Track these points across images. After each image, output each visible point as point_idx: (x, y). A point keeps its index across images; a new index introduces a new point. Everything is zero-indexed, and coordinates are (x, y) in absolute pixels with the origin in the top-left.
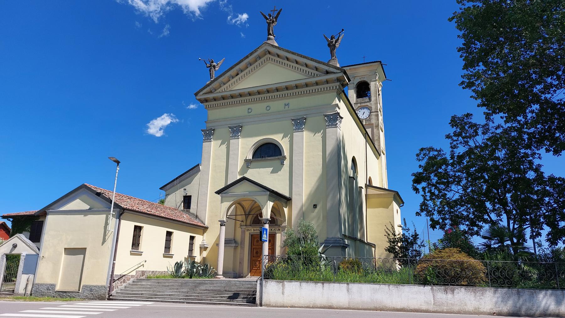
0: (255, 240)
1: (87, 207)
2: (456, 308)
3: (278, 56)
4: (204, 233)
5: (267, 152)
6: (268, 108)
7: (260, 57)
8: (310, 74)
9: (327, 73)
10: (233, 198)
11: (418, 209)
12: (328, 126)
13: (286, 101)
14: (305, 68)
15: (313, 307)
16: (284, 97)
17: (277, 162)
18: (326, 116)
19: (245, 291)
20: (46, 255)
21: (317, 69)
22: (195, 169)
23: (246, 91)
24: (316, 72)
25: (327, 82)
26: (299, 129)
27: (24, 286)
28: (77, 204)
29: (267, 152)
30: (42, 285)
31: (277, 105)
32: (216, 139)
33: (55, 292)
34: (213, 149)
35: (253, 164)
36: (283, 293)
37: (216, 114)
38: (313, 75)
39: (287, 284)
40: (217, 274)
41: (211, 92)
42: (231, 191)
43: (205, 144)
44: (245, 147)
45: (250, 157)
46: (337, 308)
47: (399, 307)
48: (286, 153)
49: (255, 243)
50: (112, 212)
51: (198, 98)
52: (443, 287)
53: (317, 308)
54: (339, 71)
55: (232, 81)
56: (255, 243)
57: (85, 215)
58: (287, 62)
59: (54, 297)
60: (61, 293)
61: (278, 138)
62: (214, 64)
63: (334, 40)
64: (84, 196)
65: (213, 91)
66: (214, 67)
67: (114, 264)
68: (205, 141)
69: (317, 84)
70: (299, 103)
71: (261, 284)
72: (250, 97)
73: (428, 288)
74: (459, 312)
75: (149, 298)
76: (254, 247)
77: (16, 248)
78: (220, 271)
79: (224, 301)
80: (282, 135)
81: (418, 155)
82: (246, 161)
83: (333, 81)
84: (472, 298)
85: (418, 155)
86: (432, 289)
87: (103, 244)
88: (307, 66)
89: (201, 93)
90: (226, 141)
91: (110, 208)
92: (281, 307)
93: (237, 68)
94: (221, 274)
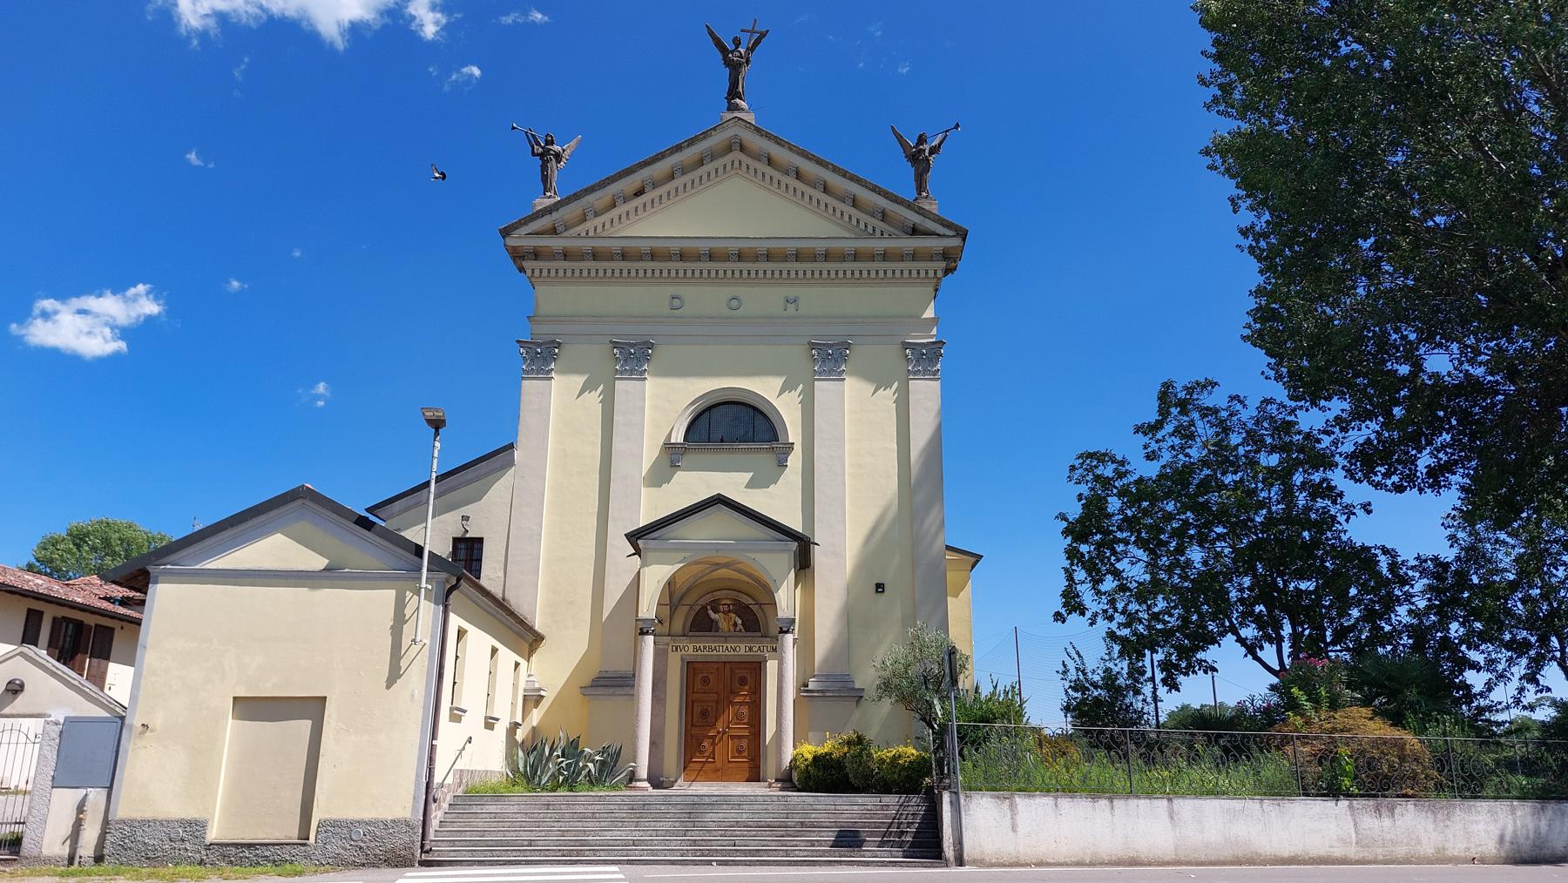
1: (320, 563)
2: (1401, 851)
3: (770, 162)
4: (530, 655)
5: (731, 426)
6: (734, 303)
7: (713, 155)
8: (862, 226)
9: (915, 231)
11: (1058, 605)
12: (915, 373)
13: (792, 292)
15: (1092, 864)
17: (766, 460)
18: (906, 346)
19: (877, 825)
20: (157, 721)
21: (884, 216)
22: (500, 456)
23: (675, 246)
24: (881, 225)
25: (914, 256)
26: (830, 372)
27: (66, 829)
28: (273, 549)
29: (731, 426)
30: (145, 823)
31: (763, 299)
32: (565, 371)
33: (209, 847)
34: (558, 408)
36: (1014, 828)
37: (560, 298)
38: (870, 229)
39: (1021, 802)
40: (632, 777)
41: (553, 231)
43: (530, 387)
44: (663, 403)
45: (678, 437)
46: (1150, 864)
47: (1286, 854)
48: (794, 434)
49: (698, 685)
50: (424, 585)
51: (511, 242)
52: (1371, 802)
53: (1102, 864)
55: (622, 209)
56: (698, 685)
57: (313, 587)
59: (201, 862)
60: (233, 850)
61: (765, 388)
62: (556, 148)
63: (926, 147)
64: (304, 526)
65: (559, 229)
66: (558, 157)
67: (433, 748)
68: (528, 374)
69: (885, 256)
70: (829, 301)
71: (956, 806)
72: (594, 264)
73: (1344, 803)
74: (1407, 861)
75: (570, 853)
76: (695, 696)
77: (21, 697)
78: (643, 772)
79: (824, 853)
80: (778, 382)
81: (1073, 468)
82: (668, 447)
83: (931, 257)
84: (1431, 826)
85: (1073, 468)
86: (1350, 807)
87: (391, 682)
88: (855, 203)
90: (602, 383)
91: (420, 569)
92: (1011, 865)
93: (638, 178)
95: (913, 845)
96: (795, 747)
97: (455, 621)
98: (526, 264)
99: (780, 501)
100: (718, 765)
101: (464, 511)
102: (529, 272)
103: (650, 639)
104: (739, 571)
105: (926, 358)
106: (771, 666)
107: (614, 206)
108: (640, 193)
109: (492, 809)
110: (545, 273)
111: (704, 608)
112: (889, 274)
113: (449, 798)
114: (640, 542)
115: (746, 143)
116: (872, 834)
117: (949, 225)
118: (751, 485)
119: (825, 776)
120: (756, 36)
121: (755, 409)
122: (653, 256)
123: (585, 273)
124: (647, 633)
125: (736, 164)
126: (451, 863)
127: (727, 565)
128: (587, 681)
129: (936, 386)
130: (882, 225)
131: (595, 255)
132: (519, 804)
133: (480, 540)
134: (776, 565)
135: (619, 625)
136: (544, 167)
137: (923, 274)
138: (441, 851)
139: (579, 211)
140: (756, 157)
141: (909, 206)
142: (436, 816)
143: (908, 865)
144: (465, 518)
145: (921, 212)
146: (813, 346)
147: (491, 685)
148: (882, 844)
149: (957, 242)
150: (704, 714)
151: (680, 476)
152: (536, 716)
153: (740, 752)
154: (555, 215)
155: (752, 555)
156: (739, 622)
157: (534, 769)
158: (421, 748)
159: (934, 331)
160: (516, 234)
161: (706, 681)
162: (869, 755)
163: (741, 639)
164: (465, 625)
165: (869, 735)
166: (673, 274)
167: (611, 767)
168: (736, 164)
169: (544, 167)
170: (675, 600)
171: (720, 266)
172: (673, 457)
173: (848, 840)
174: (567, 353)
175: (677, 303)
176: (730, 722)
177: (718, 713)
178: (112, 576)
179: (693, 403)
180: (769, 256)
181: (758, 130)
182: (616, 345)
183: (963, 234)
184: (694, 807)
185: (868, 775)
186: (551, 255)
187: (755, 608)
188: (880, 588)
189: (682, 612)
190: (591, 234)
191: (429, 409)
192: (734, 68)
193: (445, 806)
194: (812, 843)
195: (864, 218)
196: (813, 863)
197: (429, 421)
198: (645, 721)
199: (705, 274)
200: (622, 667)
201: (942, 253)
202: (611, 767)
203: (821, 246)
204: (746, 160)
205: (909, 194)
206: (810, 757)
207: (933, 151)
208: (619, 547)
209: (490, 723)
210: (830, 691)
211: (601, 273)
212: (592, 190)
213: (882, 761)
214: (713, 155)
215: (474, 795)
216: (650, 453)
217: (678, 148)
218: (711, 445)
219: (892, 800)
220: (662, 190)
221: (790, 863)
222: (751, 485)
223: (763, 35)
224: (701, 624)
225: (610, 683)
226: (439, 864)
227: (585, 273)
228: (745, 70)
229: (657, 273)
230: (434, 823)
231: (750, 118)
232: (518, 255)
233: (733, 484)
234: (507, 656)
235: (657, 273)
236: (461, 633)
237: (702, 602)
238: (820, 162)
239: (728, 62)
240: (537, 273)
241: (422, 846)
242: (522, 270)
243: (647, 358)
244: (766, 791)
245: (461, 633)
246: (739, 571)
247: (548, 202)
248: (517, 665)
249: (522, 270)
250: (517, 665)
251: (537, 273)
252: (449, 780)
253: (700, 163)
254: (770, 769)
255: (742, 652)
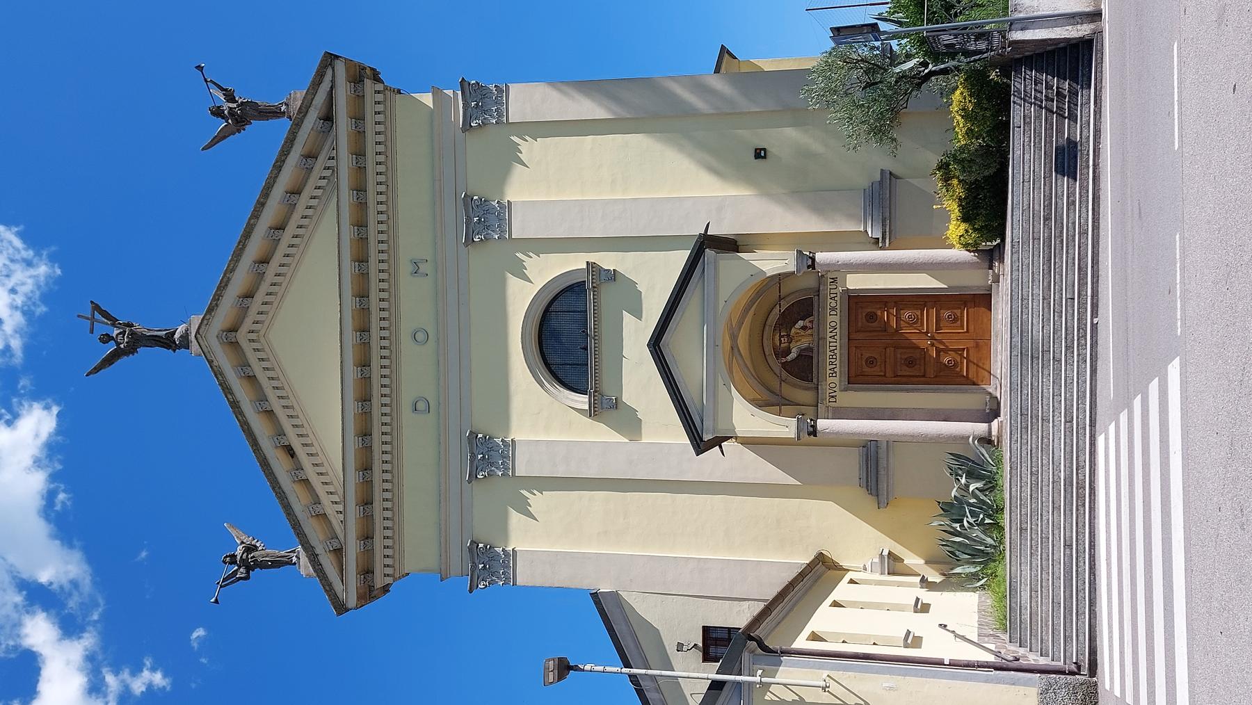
0: (866, 369)
3: (249, 295)
5: (567, 340)
6: (420, 336)
8: (323, 183)
9: (328, 117)
10: (721, 382)
12: (500, 115)
13: (405, 269)
14: (304, 200)
16: (389, 276)
17: (608, 295)
18: (467, 127)
21: (311, 156)
22: (606, 608)
24: (322, 160)
25: (358, 118)
26: (500, 218)
31: (414, 303)
34: (549, 542)
35: (608, 390)
37: (418, 544)
38: (328, 173)
40: (986, 440)
41: (338, 552)
42: (697, 401)
43: (524, 576)
44: (541, 420)
45: (582, 401)
48: (576, 262)
50: (757, 679)
51: (352, 601)
54: (329, 72)
55: (310, 472)
56: (876, 370)
58: (273, 267)
61: (520, 300)
62: (239, 551)
65: (336, 545)
66: (250, 549)
67: (953, 664)
68: (510, 579)
69: (359, 153)
78: (981, 428)
79: (1084, 188)
80: (513, 283)
82: (594, 412)
88: (296, 192)
89: (338, 587)
90: (518, 492)
91: (739, 684)
93: (271, 449)
94: (985, 425)
95: (1075, 79)
96: (951, 246)
97: (801, 643)
98: (379, 582)
99: (656, 276)
100: (971, 344)
101: (671, 649)
102: (389, 580)
103: (822, 424)
104: (741, 323)
105: (482, 102)
106: (855, 282)
107: (306, 482)
108: (290, 451)
109: (1026, 595)
110: (388, 561)
111: (784, 365)
112: (381, 148)
113: (1012, 647)
114: (706, 437)
115: (227, 325)
116: (1060, 131)
117: (320, 75)
118: (638, 315)
119: (986, 207)
120: (97, 316)
121: (547, 311)
122: (365, 433)
123: (388, 514)
124: (814, 427)
125: (253, 336)
126: (1093, 639)
127: (734, 338)
128: (870, 501)
129: (515, 90)
130: (321, 158)
131: (366, 502)
132: (1018, 566)
133: (706, 630)
134: (731, 278)
135: (802, 461)
136: (263, 565)
137: (380, 108)
138: (1077, 651)
139: (313, 522)
140: (243, 312)
141: (298, 124)
142: (1034, 659)
143: (1099, 81)
144: (680, 647)
145: (304, 110)
146: (469, 241)
147: (878, 606)
148: (1072, 117)
149: (340, 67)
150: (910, 363)
151: (629, 397)
152: (913, 560)
153: (955, 320)
154: (319, 550)
155: (721, 304)
156: (801, 323)
157: (975, 554)
158: (954, 677)
159: (449, 92)
160: (342, 596)
161: (871, 362)
162: (962, 149)
163: (821, 323)
164: (806, 632)
165: (934, 159)
166: (387, 410)
167: (974, 465)
168: (253, 336)
169: (263, 565)
170: (773, 399)
171: (375, 354)
172: (605, 406)
173: (1067, 160)
174: (483, 534)
175: (421, 406)
176: (921, 331)
177: (910, 347)
178: (562, 323)
179: (542, 385)
180: (362, 294)
181: (211, 310)
182: (473, 477)
183: (330, 59)
184: (1027, 355)
185: (985, 152)
186: (367, 554)
187: (785, 305)
188: (760, 154)
189: (787, 390)
190: (340, 508)
191: (546, 676)
192: (137, 341)
193: (1022, 651)
194: (1071, 204)
195: (313, 181)
196: (1096, 198)
197: (561, 677)
198: (917, 425)
199: (386, 372)
200: (852, 462)
201: (352, 89)
202: (974, 465)
203: (348, 232)
204: (247, 324)
205: (284, 125)
206: (963, 226)
207: (230, 97)
208: (712, 464)
209: (922, 608)
210: (885, 205)
211: (388, 495)
212: (287, 507)
213: (969, 133)
214: (243, 365)
215: (1008, 621)
216: (601, 433)
217: (235, 405)
218: (591, 362)
219: (1017, 114)
220: (286, 425)
221: (1096, 227)
222: (638, 315)
223: (96, 307)
224: (804, 369)
225: (873, 472)
226: (1093, 652)
227: (388, 514)
228: (139, 327)
229: (386, 429)
230: (1044, 662)
231: (196, 320)
232: (368, 594)
233: (635, 334)
234: (842, 591)
235: (386, 429)
236: (815, 637)
237: (777, 367)
238: (247, 235)
239: (131, 349)
240: (389, 571)
241: (1072, 673)
242: (386, 589)
243: (488, 440)
244: (1005, 285)
245: (815, 637)
246: (741, 323)
247: (304, 559)
248: (852, 582)
249: (386, 589)
250: (852, 582)
251: (389, 571)
252: (992, 647)
253: (252, 379)
254: (974, 280)
255: (837, 319)
